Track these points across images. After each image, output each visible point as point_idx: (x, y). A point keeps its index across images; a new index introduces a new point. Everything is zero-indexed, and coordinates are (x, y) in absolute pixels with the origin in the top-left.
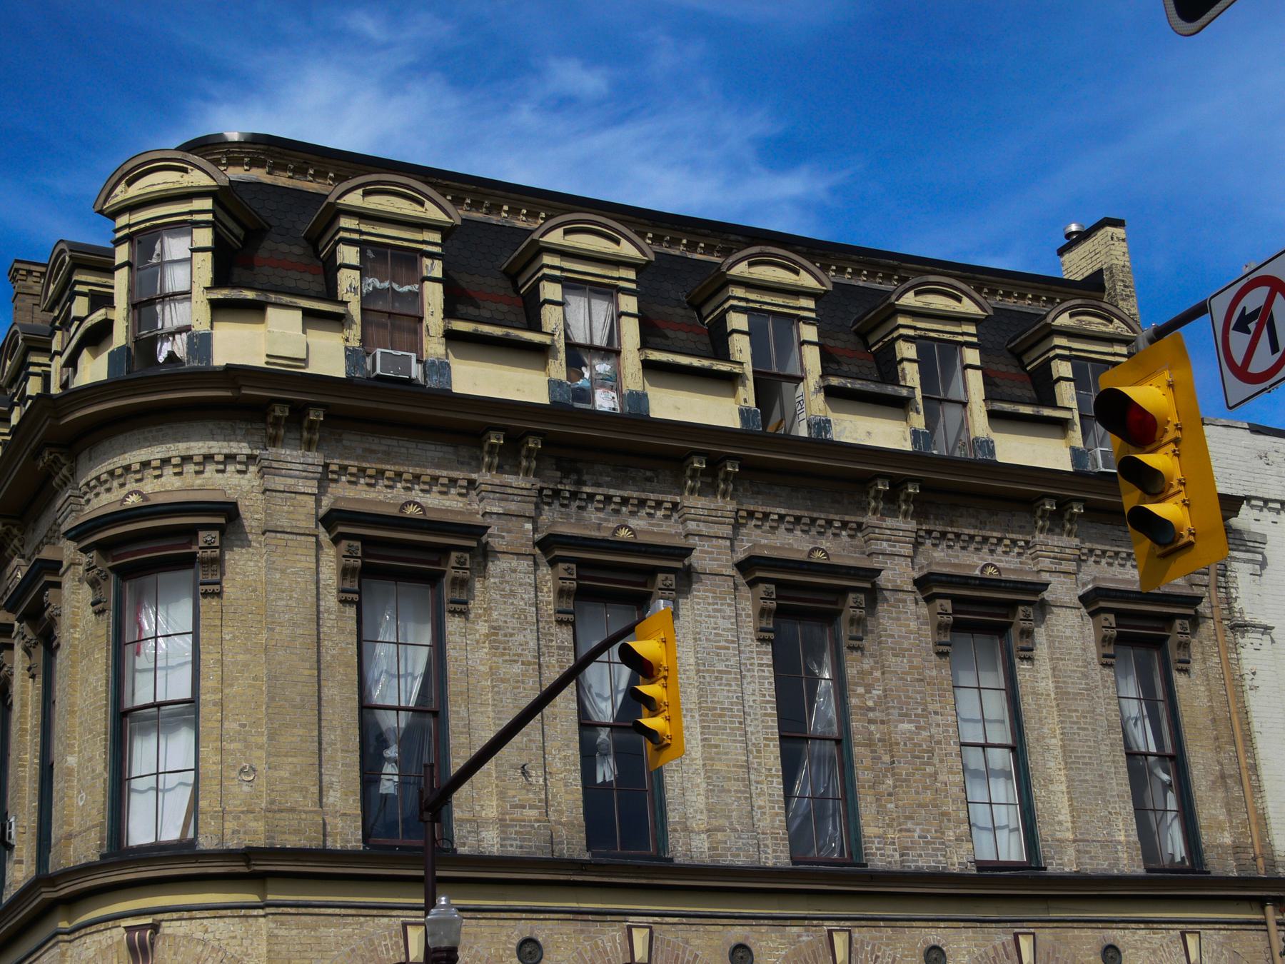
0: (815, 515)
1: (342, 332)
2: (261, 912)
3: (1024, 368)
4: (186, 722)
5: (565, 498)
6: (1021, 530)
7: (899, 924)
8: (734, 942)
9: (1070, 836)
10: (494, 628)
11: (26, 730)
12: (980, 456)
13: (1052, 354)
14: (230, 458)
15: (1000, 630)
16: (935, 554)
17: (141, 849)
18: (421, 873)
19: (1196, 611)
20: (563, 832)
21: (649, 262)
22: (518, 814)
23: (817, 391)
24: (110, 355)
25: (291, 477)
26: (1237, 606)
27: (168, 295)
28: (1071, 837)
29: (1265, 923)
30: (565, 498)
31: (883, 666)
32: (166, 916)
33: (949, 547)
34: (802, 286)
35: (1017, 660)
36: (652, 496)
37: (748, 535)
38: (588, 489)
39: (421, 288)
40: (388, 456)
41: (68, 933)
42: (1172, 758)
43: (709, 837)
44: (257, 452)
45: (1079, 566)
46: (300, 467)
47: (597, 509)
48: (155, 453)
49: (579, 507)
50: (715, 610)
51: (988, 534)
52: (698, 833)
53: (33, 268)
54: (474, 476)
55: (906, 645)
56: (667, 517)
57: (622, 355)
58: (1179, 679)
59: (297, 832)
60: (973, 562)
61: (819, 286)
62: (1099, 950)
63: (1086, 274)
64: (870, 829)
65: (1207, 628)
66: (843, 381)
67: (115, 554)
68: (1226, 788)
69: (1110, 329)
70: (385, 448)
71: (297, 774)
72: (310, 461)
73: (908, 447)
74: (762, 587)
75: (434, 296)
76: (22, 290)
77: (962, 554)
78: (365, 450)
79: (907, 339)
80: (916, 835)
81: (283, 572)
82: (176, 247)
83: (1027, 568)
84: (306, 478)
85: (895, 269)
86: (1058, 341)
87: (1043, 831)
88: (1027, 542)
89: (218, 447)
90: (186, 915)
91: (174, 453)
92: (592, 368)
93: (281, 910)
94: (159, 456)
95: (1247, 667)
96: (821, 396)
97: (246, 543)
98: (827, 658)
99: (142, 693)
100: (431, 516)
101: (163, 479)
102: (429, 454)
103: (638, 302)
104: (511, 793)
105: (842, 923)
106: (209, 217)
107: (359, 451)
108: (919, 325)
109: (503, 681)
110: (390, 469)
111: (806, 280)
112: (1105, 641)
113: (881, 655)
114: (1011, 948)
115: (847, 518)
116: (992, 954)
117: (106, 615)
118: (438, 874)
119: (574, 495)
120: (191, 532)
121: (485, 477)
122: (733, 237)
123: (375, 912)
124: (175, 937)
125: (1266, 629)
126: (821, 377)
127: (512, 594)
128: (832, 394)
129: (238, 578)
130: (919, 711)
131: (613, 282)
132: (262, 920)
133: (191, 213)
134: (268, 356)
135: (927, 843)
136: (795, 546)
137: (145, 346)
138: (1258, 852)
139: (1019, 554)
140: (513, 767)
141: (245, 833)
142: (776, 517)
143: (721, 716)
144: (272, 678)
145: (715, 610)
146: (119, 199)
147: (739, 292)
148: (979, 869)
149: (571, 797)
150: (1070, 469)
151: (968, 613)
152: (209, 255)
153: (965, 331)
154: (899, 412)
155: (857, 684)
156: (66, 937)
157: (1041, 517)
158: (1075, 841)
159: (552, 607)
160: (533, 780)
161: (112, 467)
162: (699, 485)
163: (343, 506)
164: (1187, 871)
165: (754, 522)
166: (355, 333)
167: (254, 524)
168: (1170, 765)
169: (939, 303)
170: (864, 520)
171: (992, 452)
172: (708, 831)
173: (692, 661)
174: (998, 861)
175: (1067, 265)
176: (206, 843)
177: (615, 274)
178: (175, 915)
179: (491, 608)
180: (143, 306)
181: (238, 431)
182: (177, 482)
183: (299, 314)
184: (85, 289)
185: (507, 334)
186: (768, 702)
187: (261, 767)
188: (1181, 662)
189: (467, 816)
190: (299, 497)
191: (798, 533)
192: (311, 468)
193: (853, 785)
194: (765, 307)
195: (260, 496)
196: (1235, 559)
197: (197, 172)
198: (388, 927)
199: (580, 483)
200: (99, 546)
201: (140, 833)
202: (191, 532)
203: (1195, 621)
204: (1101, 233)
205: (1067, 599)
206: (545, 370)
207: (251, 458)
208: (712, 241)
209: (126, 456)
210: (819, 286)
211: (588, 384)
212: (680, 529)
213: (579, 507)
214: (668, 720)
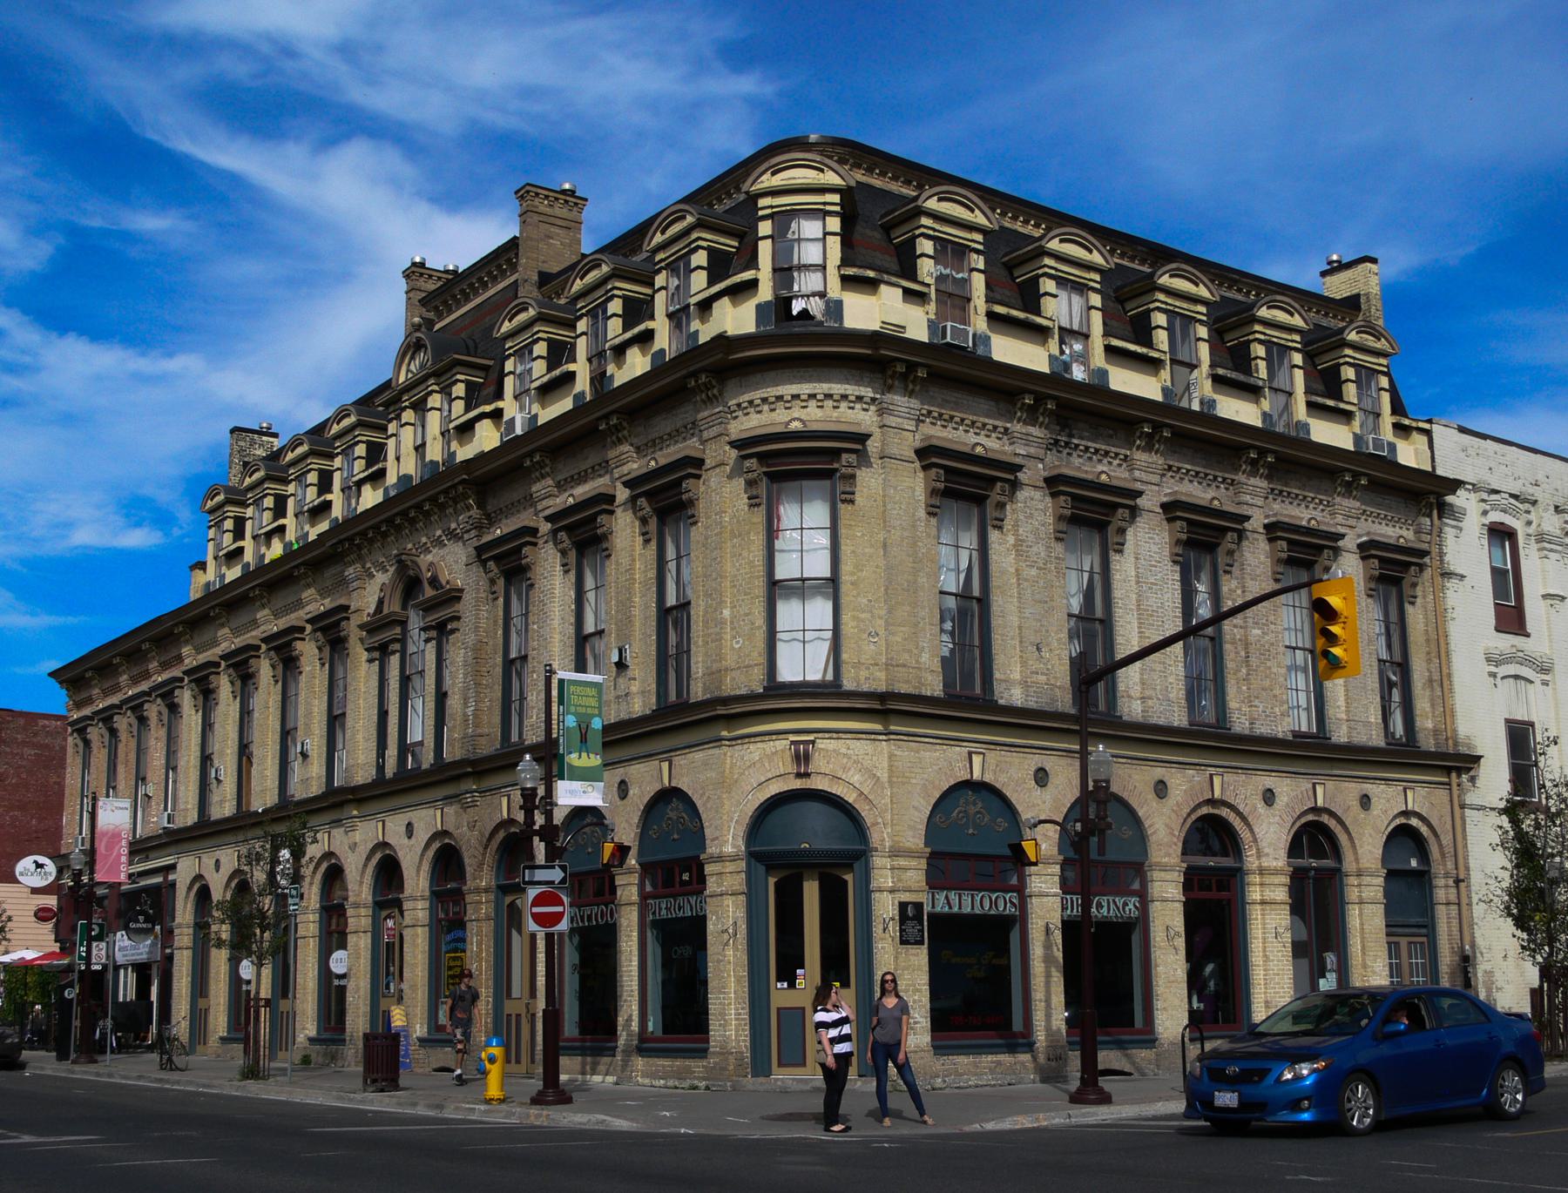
0: (1208, 471)
1: (923, 306)
2: (884, 737)
3: (1014, 279)
4: (825, 596)
5: (1061, 446)
6: (1326, 493)
7: (1250, 772)
8: (1156, 779)
9: (1344, 716)
10: (1021, 540)
11: (635, 579)
12: (1302, 435)
13: (917, 232)
14: (859, 399)
15: (980, 501)
16: (1275, 506)
17: (792, 685)
18: (1078, 728)
19: (1016, 477)
20: (1058, 692)
21: (1110, 269)
22: (1035, 678)
23: (1208, 378)
24: (759, 307)
25: (899, 417)
26: (1446, 559)
27: (804, 266)
28: (1345, 717)
29: (1449, 784)
30: (1061, 446)
31: (1244, 587)
32: (820, 735)
33: (1283, 501)
34: (1200, 296)
35: (1221, 572)
36: (1113, 449)
37: (1167, 483)
38: (1075, 441)
39: (970, 276)
40: (957, 406)
41: (729, 740)
42: (1399, 665)
43: (1143, 703)
44: (878, 396)
45: (917, 426)
46: (906, 410)
47: (1079, 456)
48: (805, 389)
49: (1068, 454)
50: (1149, 538)
51: (1307, 494)
52: (1136, 700)
53: (539, 191)
54: (1009, 425)
55: (1258, 573)
56: (1120, 465)
57: (1091, 339)
58: (1409, 609)
59: (907, 682)
60: (1303, 515)
61: (1211, 297)
62: (1358, 798)
63: (1344, 296)
64: (1233, 704)
65: (1428, 573)
66: (1225, 371)
67: (770, 462)
68: (1432, 689)
69: (1378, 345)
70: (954, 399)
71: (905, 639)
72: (912, 406)
73: (1259, 424)
74: (1179, 523)
75: (978, 282)
76: (529, 208)
77: (1290, 507)
78: (943, 400)
79: (1261, 342)
80: (1260, 710)
81: (895, 488)
82: (811, 228)
83: (1326, 520)
84: (908, 418)
85: (1236, 282)
86: (1048, 261)
87: (1330, 712)
88: (1328, 502)
89: (851, 390)
90: (835, 735)
91: (819, 391)
92: (1071, 347)
93: (899, 737)
94: (807, 392)
95: (1450, 602)
96: (1209, 382)
97: (869, 465)
98: (1205, 576)
99: (786, 568)
100: (990, 455)
101: (808, 409)
102: (982, 406)
103: (841, 222)
104: (1031, 663)
105: (1218, 769)
106: (838, 208)
107: (940, 400)
108: (1268, 332)
109: (1026, 580)
110: (958, 415)
111: (1203, 292)
112: (934, 492)
113: (1243, 578)
114: (1311, 793)
115: (1226, 475)
116: (1300, 797)
117: (760, 508)
118: (1090, 729)
119: (1067, 444)
120: (836, 454)
121: (1017, 427)
122: (1140, 248)
123: (952, 743)
124: (827, 751)
125: (1462, 577)
126: (1210, 366)
127: (1031, 516)
128: (1217, 380)
129: (865, 490)
130: (1264, 621)
131: (1086, 282)
132: (884, 743)
133: (825, 204)
134: (883, 322)
135: (1267, 716)
136: (1194, 493)
137: (783, 303)
138: (1449, 735)
139: (1299, 505)
140: (1032, 644)
141: (874, 680)
142: (1184, 471)
143: (1152, 616)
144: (889, 568)
145: (1149, 538)
146: (762, 186)
147: (1161, 297)
148: (1294, 736)
149: (1062, 668)
150: (1352, 449)
151: (1087, 511)
152: (839, 238)
153: (974, 238)
154: (1252, 396)
155: (1228, 599)
156: (727, 743)
157: (1020, 409)
158: (1347, 721)
159: (1051, 527)
160: (1043, 654)
161: (766, 395)
162: (1143, 444)
163: (935, 442)
164: (1402, 745)
165: (1170, 474)
166: (932, 307)
167: (874, 450)
168: (1398, 670)
169: (1281, 316)
170: (1236, 477)
171: (1308, 432)
172: (1142, 698)
173: (1133, 574)
174: (1300, 731)
175: (1328, 285)
176: (848, 685)
177: (1087, 276)
178: (827, 735)
179: (1018, 526)
180: (784, 272)
181: (865, 379)
182: (819, 414)
183: (900, 291)
184: (704, 244)
185: (1027, 318)
186: (1177, 607)
187: (882, 632)
188: (997, 519)
189: (1003, 677)
190: (905, 433)
191: (1196, 484)
192: (912, 412)
193: (1222, 671)
194: (1176, 310)
195: (878, 430)
196: (1447, 525)
197: (831, 173)
198: (960, 754)
199: (1071, 436)
200: (762, 457)
201: (788, 672)
202: (836, 454)
203: (1421, 567)
204: (1361, 267)
205: (1350, 546)
206: (1044, 345)
207: (873, 400)
208: (1125, 249)
209: (779, 388)
210: (1211, 297)
211: (1068, 359)
212: (1126, 475)
213: (1068, 454)
214: (1345, 650)
